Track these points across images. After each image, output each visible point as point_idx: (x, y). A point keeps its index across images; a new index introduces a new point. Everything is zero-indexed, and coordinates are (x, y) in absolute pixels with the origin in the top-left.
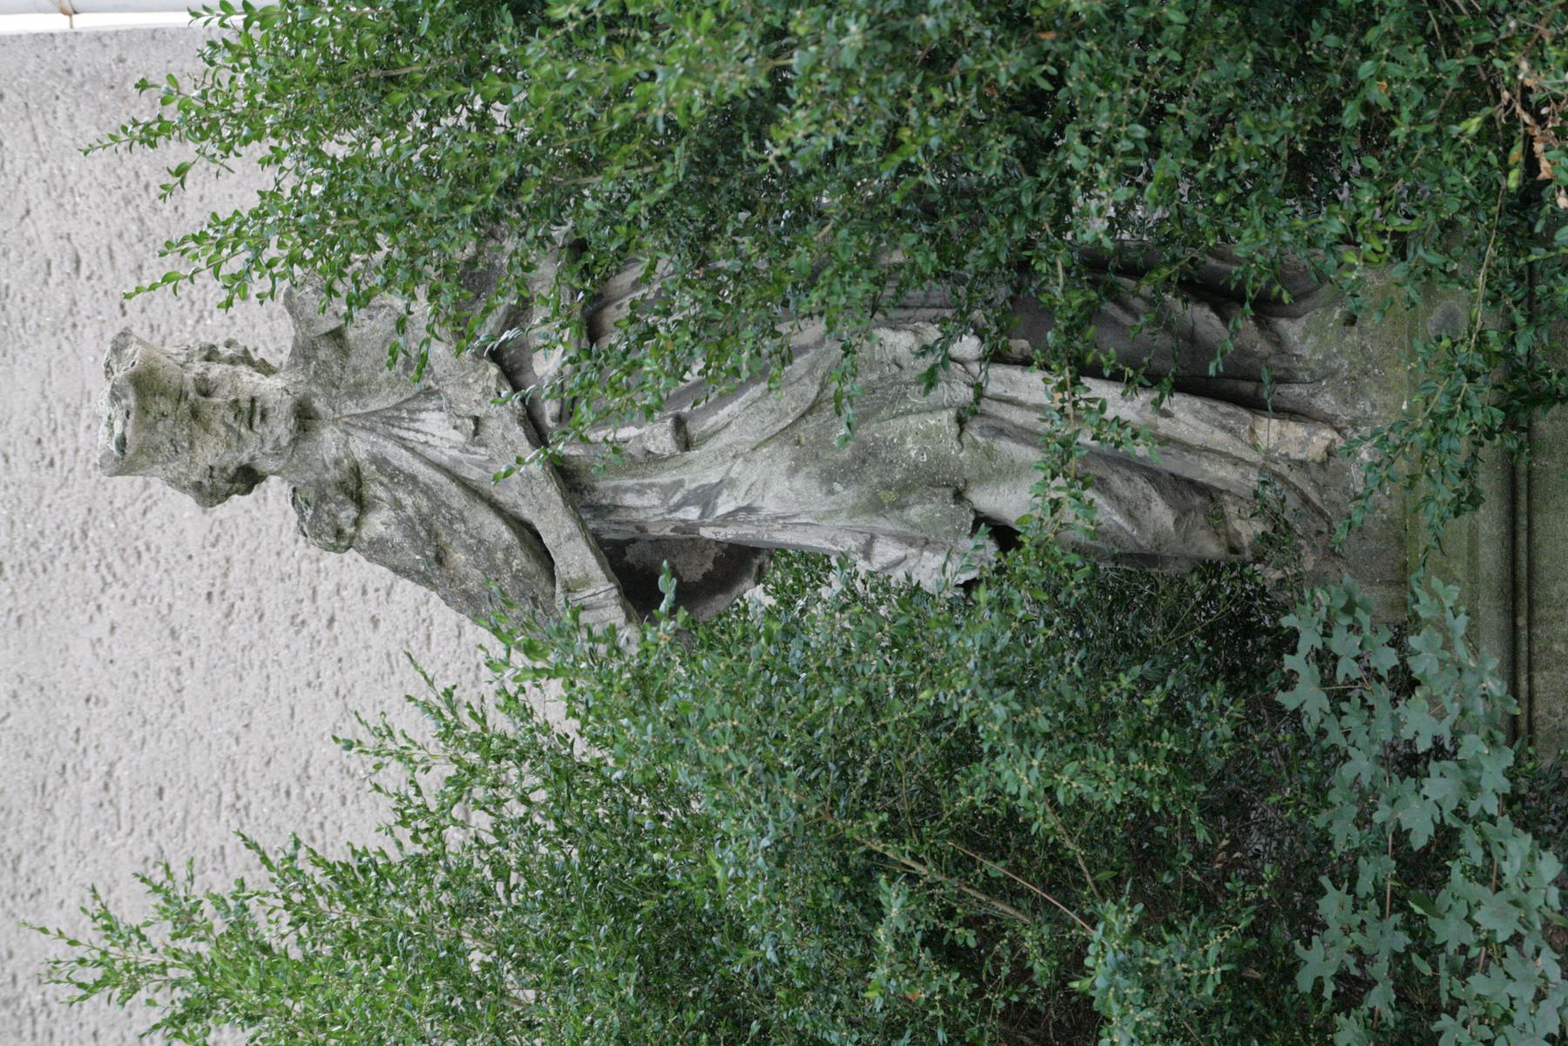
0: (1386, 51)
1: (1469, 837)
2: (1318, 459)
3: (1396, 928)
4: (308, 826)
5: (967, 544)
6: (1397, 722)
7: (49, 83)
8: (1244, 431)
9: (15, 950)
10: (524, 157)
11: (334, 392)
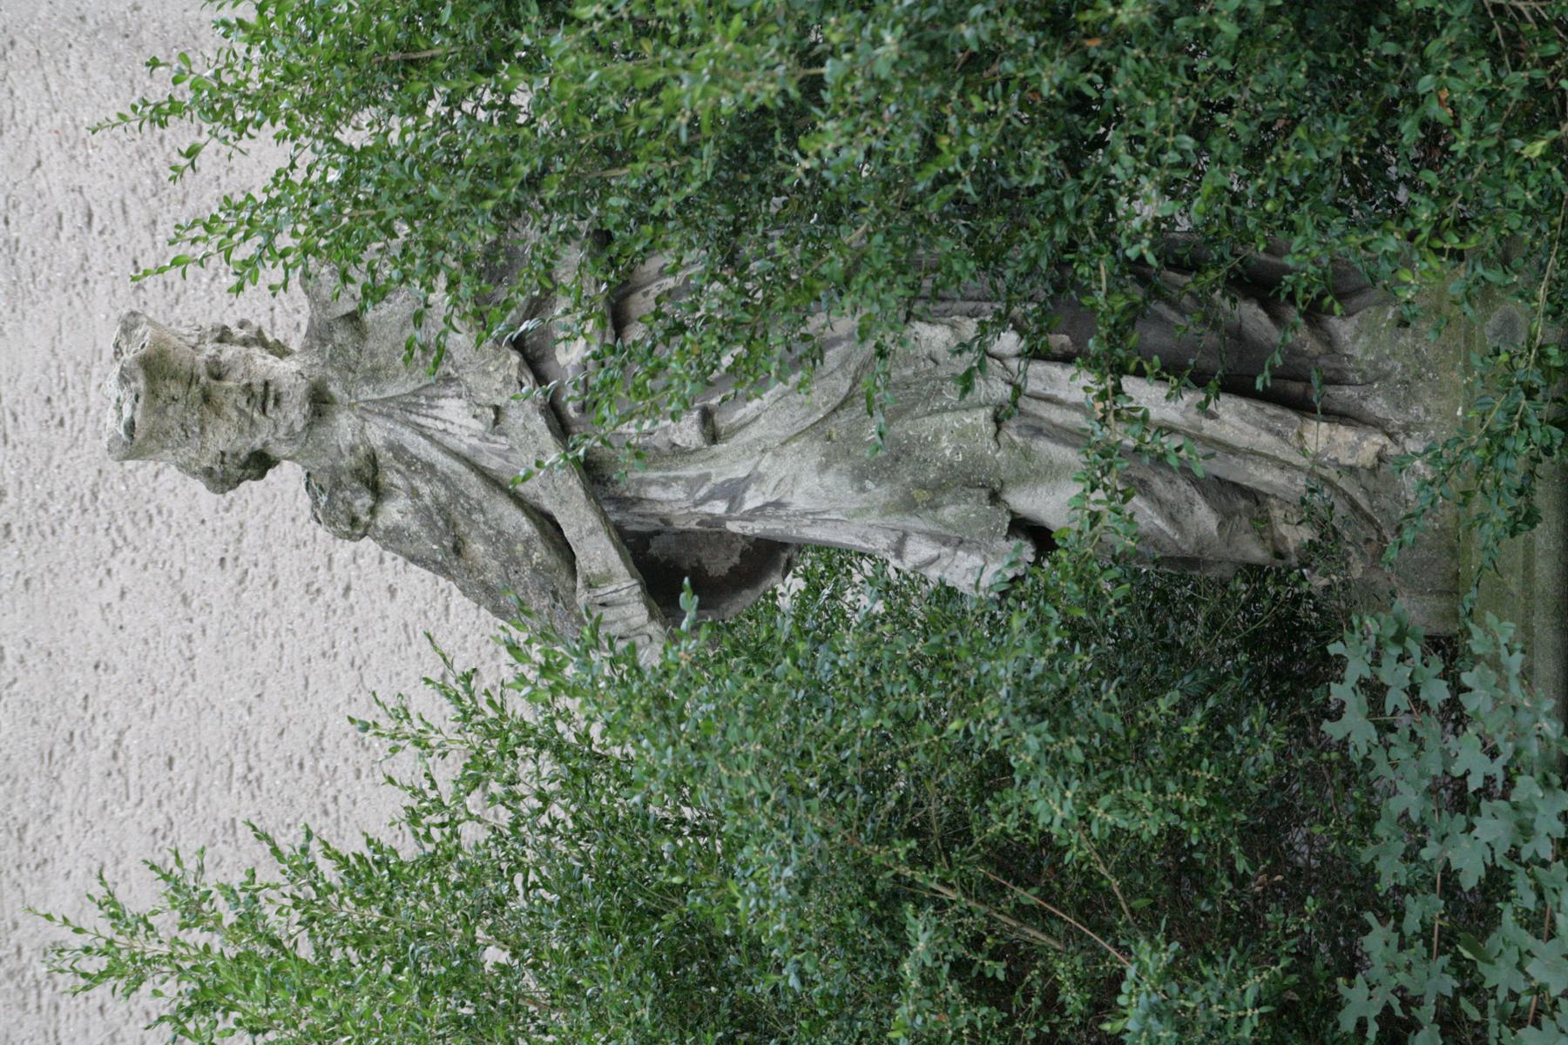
0: (1447, 65)
1: (1521, 881)
2: (1369, 465)
3: (1443, 971)
4: (322, 799)
5: (1002, 544)
6: (1448, 758)
7: (62, 30)
8: (1292, 434)
9: (21, 922)
10: (547, 149)
11: (350, 376)
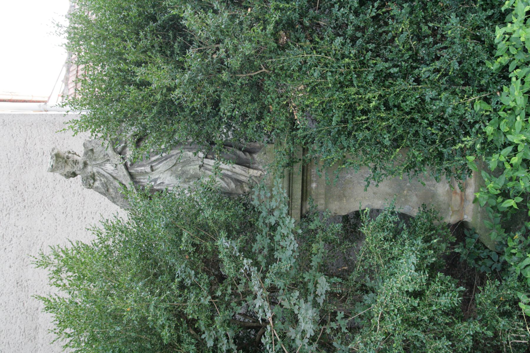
8: (247, 171)
